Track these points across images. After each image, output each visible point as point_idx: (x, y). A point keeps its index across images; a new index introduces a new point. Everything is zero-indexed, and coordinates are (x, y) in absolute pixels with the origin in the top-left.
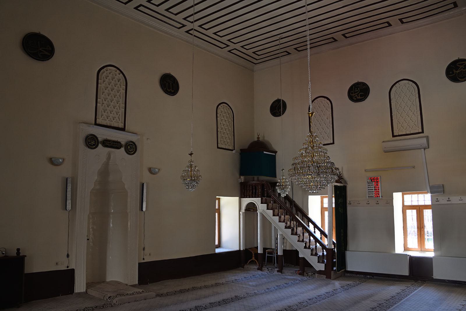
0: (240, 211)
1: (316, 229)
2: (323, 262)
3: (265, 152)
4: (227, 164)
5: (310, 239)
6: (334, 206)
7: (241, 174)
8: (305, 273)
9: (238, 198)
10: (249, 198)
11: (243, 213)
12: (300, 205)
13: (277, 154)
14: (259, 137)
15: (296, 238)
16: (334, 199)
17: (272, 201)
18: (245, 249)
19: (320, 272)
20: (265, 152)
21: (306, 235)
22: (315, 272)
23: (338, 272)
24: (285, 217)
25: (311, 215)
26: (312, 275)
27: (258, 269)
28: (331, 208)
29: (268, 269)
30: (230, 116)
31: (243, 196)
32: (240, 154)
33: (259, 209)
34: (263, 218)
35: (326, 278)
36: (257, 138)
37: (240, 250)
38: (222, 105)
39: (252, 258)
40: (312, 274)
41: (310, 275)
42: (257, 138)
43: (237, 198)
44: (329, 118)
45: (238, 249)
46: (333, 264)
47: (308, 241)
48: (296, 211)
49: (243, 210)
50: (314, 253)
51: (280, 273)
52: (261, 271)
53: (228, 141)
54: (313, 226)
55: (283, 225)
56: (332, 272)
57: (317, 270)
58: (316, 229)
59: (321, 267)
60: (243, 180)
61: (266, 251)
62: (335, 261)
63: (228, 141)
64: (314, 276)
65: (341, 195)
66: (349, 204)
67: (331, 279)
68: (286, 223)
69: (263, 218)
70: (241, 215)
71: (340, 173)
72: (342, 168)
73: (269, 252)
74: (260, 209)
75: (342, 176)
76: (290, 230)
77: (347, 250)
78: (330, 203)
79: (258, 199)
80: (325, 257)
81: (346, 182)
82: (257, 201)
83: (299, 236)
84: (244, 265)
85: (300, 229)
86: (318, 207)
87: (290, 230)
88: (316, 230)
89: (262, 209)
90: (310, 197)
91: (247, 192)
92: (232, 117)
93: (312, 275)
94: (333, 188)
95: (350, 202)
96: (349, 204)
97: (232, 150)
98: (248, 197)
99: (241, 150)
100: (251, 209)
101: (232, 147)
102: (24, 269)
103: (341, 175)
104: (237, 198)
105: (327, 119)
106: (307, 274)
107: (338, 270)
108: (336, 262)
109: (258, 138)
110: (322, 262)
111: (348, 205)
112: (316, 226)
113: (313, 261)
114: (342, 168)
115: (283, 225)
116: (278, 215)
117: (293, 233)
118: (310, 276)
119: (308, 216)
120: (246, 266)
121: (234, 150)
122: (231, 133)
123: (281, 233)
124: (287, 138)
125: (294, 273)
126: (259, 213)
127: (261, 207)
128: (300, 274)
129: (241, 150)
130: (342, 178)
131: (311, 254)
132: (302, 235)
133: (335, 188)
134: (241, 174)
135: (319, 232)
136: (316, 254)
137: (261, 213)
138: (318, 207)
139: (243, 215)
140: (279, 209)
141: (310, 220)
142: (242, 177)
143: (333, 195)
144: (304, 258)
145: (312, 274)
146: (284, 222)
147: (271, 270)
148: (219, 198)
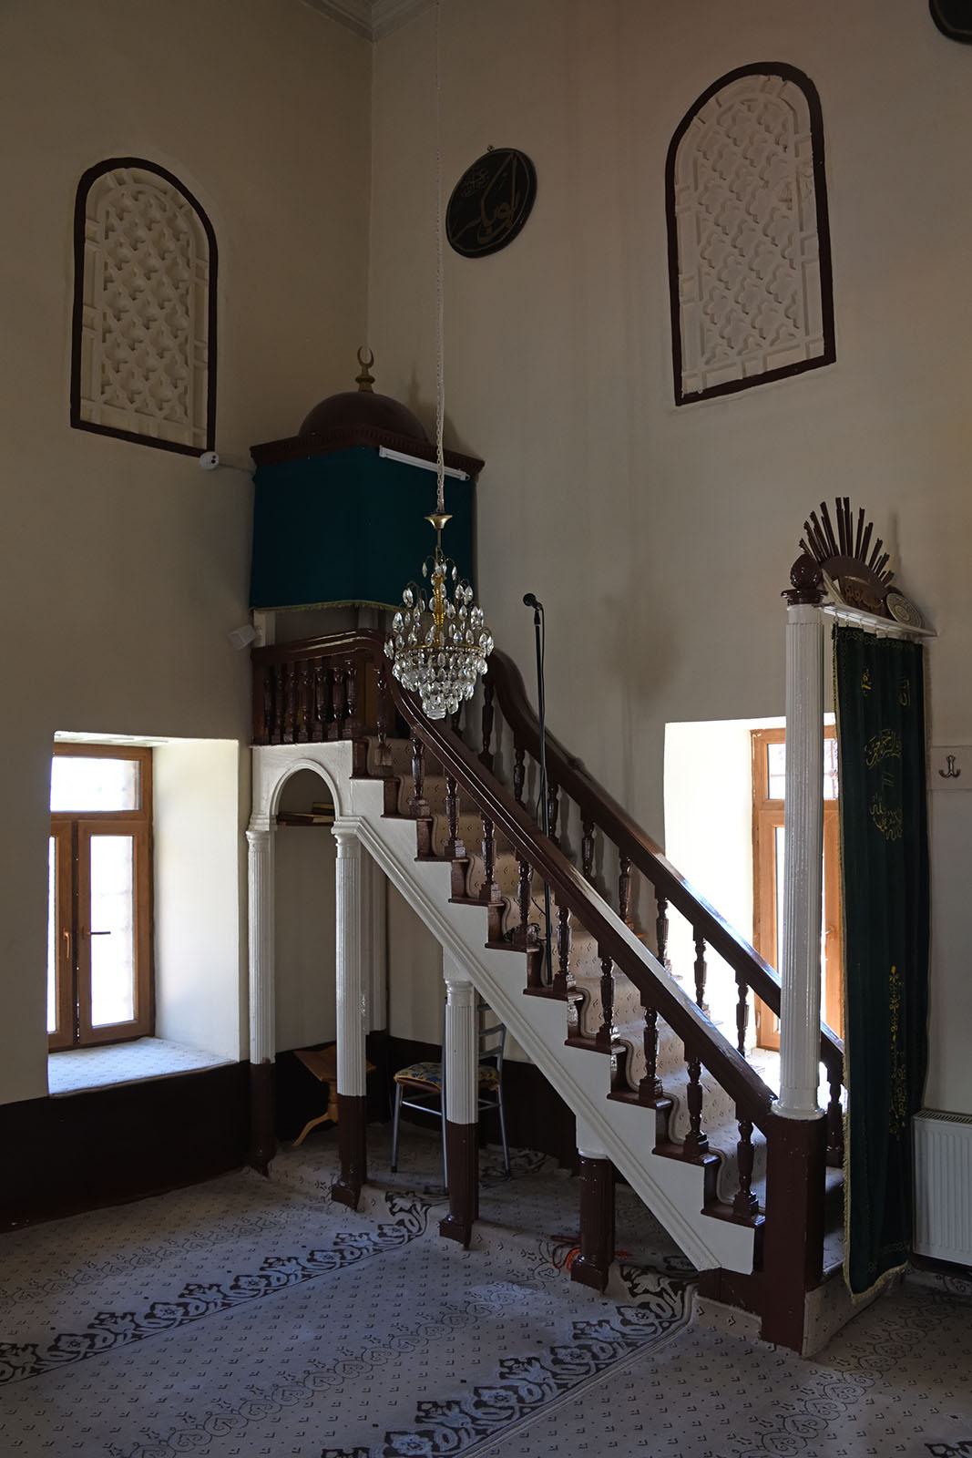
0: (245, 822)
1: (707, 945)
2: (742, 1213)
3: (385, 452)
4: (166, 531)
5: (651, 1036)
6: (831, 790)
7: (258, 597)
8: (614, 1273)
9: (234, 744)
10: (296, 741)
11: (262, 836)
12: (611, 783)
13: (483, 475)
14: (371, 372)
15: (559, 1014)
16: (831, 747)
17: (418, 757)
18: (278, 1056)
19: (719, 1284)
20: (385, 452)
21: (626, 992)
22: (678, 1272)
23: (856, 1291)
24: (489, 866)
25: (678, 855)
26: (659, 1294)
27: (338, 1195)
28: (812, 808)
29: (394, 1206)
30: (191, 252)
31: (264, 732)
32: (254, 479)
33: (341, 815)
34: (366, 865)
35: (765, 1336)
36: (358, 380)
37: (245, 1064)
38: (122, 172)
39: (325, 1110)
40: (665, 1283)
41: (646, 1291)
42: (358, 380)
43: (228, 749)
44: (795, 198)
45: (237, 1059)
46: (823, 1213)
47: (638, 1041)
48: (581, 823)
49: (263, 822)
50: (682, 1130)
51: (455, 1246)
52: (355, 1208)
53: (168, 392)
54: (691, 927)
55: (476, 920)
56: (812, 1300)
57: (702, 1263)
58: (707, 945)
59: (728, 1247)
60: (262, 633)
61: (397, 1077)
62: (838, 1189)
63: (168, 392)
64: (678, 1306)
65: (880, 698)
66: (942, 773)
67: (797, 1347)
68: (502, 910)
69: (366, 865)
70: (251, 848)
71: (881, 553)
72: (894, 522)
73: (412, 1087)
74: (348, 811)
75: (891, 575)
76: (517, 964)
77: (927, 1103)
78: (805, 771)
79: (308, 748)
80: (760, 1166)
81: (917, 615)
82: (331, 758)
83: (579, 1005)
84: (272, 1156)
85: (586, 950)
86: (723, 800)
87: (517, 964)
88: (711, 954)
89: (361, 811)
90: (676, 734)
91: (284, 710)
92: (199, 256)
93: (659, 1294)
94: (829, 644)
95: (950, 760)
96: (942, 773)
97: (196, 452)
98: (286, 738)
99: (258, 452)
100: (305, 806)
101: (195, 436)
102: (134, 946)
103: (886, 568)
104: (233, 745)
105: (783, 206)
106: (627, 1278)
107: (864, 1266)
108: (837, 1195)
109: (366, 380)
110: (735, 1205)
111: (935, 782)
112: (707, 929)
113: (671, 1193)
114: (894, 522)
115: (476, 920)
116: (449, 855)
117: (544, 979)
118: (647, 1298)
119: (658, 857)
120: (278, 1165)
121: (211, 447)
122: (189, 349)
123: (464, 977)
124: (521, 368)
125: (543, 1261)
126: (339, 841)
127: (358, 801)
128: (579, 1274)
129: (258, 452)
130: (892, 590)
131: (658, 1141)
132: (596, 993)
133: (838, 650)
134: (258, 597)
135: (731, 972)
136: (693, 1149)
137: (351, 840)
138: (723, 800)
139: (262, 850)
140: (453, 815)
141: (670, 889)
142: (261, 618)
143: (830, 719)
144: (606, 1166)
145: (665, 1283)
146: (483, 899)
147: (409, 1211)
148: (150, 750)
